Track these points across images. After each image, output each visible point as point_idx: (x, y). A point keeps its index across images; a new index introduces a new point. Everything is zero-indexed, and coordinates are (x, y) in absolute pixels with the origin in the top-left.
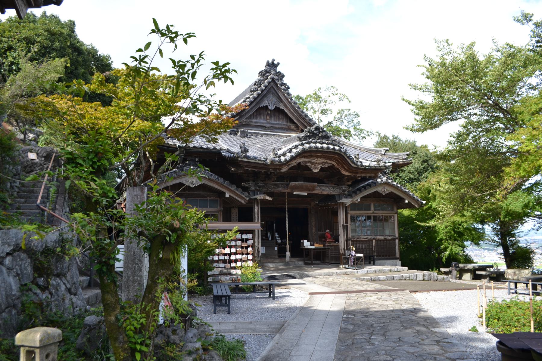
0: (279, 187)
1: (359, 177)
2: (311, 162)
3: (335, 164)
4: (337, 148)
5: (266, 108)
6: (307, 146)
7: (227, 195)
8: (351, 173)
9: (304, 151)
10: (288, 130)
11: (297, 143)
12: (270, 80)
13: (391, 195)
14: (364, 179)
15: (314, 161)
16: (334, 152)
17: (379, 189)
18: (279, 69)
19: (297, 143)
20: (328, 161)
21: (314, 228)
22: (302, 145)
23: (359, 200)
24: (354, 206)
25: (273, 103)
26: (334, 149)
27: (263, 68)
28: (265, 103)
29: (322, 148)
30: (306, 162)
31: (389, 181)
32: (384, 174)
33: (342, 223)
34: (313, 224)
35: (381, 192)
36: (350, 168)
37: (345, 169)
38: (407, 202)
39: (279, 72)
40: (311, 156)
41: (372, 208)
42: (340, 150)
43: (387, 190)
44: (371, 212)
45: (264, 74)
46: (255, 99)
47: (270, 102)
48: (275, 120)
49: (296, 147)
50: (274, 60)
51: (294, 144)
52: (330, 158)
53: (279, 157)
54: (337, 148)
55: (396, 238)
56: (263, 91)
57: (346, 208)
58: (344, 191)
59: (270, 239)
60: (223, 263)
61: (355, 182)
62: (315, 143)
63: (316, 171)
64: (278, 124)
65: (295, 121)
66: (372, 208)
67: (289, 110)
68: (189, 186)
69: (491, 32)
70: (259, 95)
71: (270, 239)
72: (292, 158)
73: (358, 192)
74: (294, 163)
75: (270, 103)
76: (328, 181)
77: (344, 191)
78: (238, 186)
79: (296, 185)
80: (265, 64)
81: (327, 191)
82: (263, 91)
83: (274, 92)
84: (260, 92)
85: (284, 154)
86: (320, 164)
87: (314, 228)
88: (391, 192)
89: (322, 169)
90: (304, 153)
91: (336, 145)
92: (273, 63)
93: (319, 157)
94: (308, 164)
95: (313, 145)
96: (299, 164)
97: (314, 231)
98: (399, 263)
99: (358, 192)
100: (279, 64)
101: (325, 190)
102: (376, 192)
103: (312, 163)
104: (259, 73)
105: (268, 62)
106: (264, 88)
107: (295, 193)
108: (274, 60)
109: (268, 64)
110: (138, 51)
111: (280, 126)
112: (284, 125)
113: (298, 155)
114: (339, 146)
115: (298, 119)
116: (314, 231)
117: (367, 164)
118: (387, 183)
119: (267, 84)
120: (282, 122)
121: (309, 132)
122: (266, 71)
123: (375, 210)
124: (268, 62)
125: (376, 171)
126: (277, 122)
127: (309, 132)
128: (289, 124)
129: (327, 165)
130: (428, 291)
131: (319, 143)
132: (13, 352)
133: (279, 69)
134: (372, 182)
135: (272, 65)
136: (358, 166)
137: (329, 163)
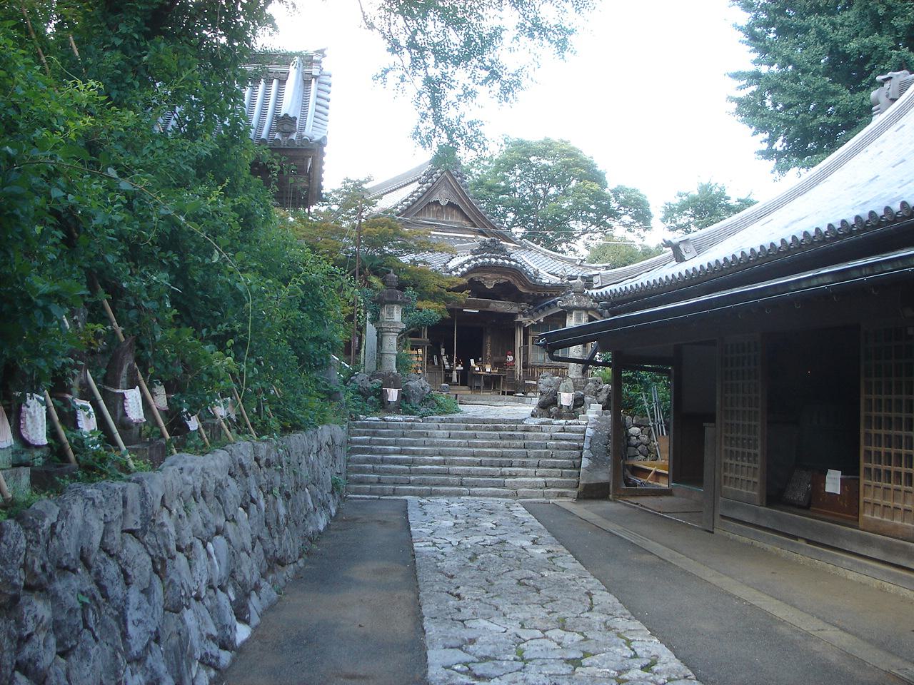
3: (510, 279)
4: (513, 263)
5: (437, 203)
6: (481, 261)
9: (476, 267)
11: (470, 257)
16: (510, 267)
19: (470, 257)
22: (475, 259)
24: (536, 327)
26: (510, 264)
28: (436, 198)
30: (479, 278)
36: (527, 285)
46: (424, 193)
48: (447, 218)
49: (469, 262)
51: (466, 258)
52: (506, 274)
53: (450, 272)
54: (513, 263)
59: (436, 364)
64: (451, 223)
70: (428, 188)
71: (436, 364)
72: (464, 274)
75: (442, 197)
84: (430, 184)
85: (456, 269)
89: (496, 285)
90: (476, 269)
91: (513, 260)
94: (482, 280)
95: (487, 260)
97: (488, 354)
99: (540, 311)
103: (486, 279)
106: (435, 180)
110: (293, 4)
113: (470, 271)
114: (516, 261)
116: (488, 354)
119: (439, 175)
120: (456, 220)
125: (558, 289)
128: (464, 222)
129: (502, 281)
131: (494, 257)
132: (0, 146)
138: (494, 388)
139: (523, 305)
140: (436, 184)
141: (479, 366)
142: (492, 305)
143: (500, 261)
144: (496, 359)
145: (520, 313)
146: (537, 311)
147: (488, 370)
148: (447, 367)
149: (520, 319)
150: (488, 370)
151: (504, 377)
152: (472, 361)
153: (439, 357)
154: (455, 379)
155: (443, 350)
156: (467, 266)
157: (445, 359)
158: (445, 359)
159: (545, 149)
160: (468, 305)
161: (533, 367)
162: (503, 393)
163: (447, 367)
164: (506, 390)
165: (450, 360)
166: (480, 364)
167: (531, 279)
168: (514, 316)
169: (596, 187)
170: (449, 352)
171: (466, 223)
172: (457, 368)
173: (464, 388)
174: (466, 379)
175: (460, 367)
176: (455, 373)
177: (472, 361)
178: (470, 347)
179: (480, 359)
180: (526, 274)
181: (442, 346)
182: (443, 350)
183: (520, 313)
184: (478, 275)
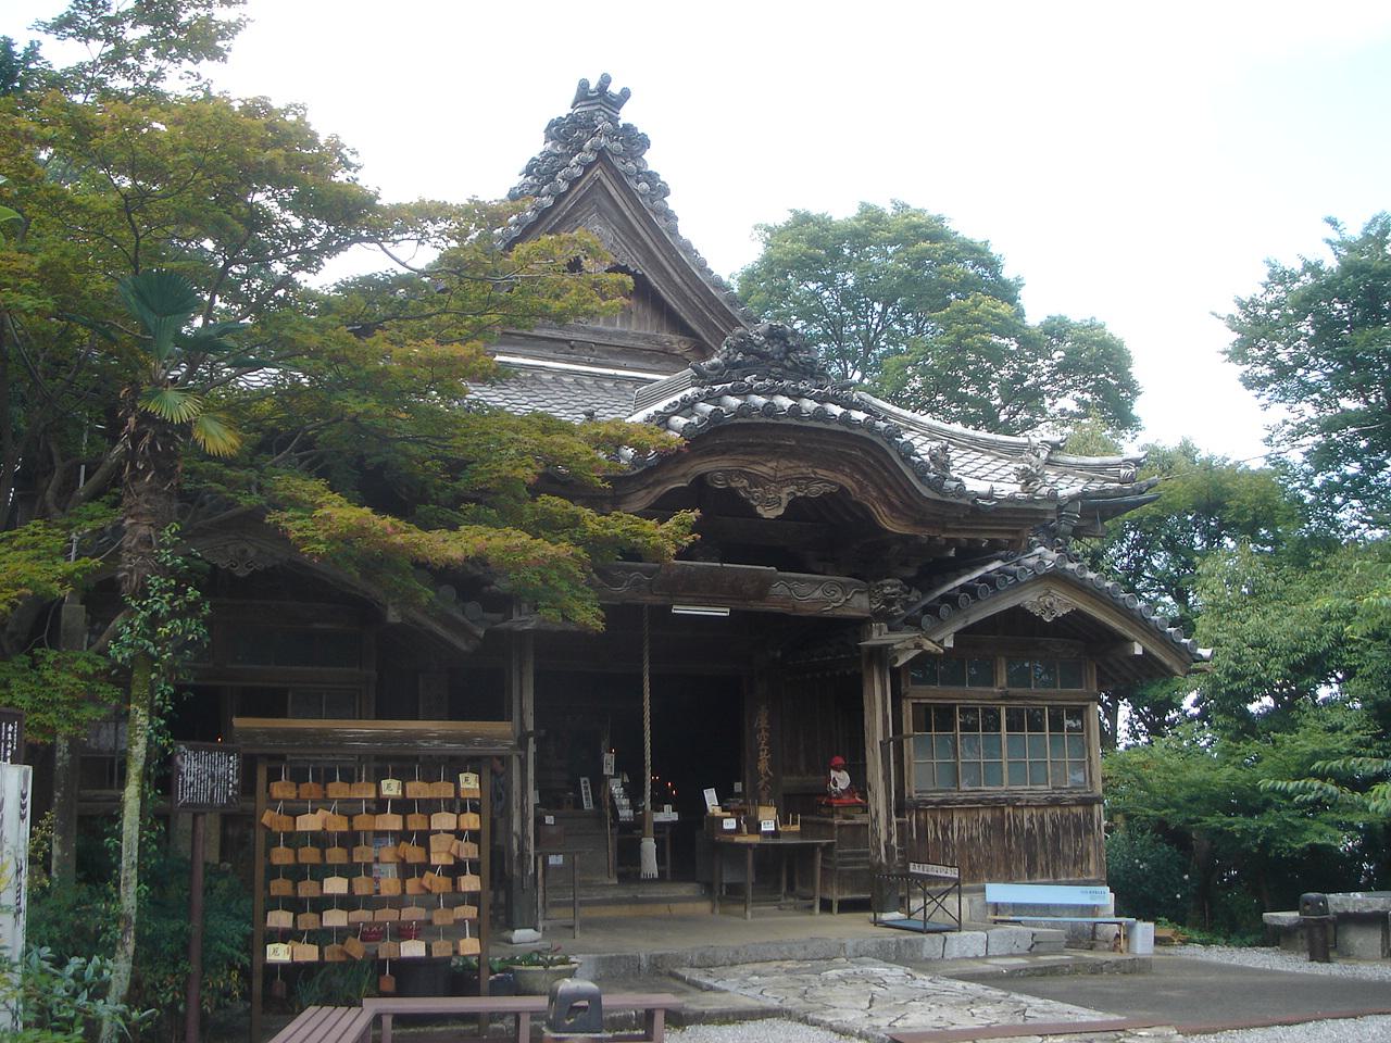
1: (950, 543)
2: (748, 475)
3: (849, 483)
4: (859, 416)
8: (917, 523)
10: (662, 357)
12: (591, 157)
13: (1075, 628)
14: (972, 556)
15: (764, 469)
17: (1030, 599)
18: (626, 115)
20: (821, 472)
21: (763, 756)
23: (949, 644)
27: (563, 108)
29: (795, 411)
30: (728, 473)
31: (1069, 566)
32: (1052, 537)
33: (879, 737)
35: (1037, 612)
36: (909, 504)
37: (891, 506)
38: (1138, 650)
39: (628, 128)
41: (1002, 679)
42: (871, 427)
43: (1061, 603)
45: (560, 131)
49: (686, 407)
50: (606, 80)
56: (559, 198)
57: (896, 674)
58: (889, 603)
59: (588, 805)
60: (341, 908)
61: (934, 568)
62: (769, 392)
63: (769, 513)
64: (623, 335)
65: (695, 326)
66: (1002, 679)
67: (669, 279)
69: (1303, 230)
71: (588, 805)
73: (944, 609)
77: (889, 603)
80: (572, 94)
82: (559, 198)
83: (606, 204)
84: (548, 201)
87: (763, 756)
88: (1077, 613)
89: (794, 504)
90: (713, 437)
91: (857, 407)
94: (740, 483)
97: (763, 766)
98: (1307, 955)
99: (944, 609)
101: (814, 593)
102: (1019, 611)
103: (755, 480)
104: (551, 125)
105: (584, 85)
106: (564, 187)
107: (678, 610)
108: (606, 80)
109: (583, 94)
111: (629, 343)
112: (646, 337)
115: (701, 318)
116: (763, 766)
117: (981, 487)
118: (1057, 577)
119: (578, 172)
121: (740, 347)
122: (573, 118)
123: (1010, 683)
124: (584, 85)
126: (618, 327)
127: (740, 347)
129: (816, 490)
130: (1248, 1027)
133: (626, 115)
134: (999, 570)
135: (599, 101)
136: (945, 494)
137: (823, 481)
138: (791, 887)
139: (890, 587)
140: (568, 203)
141: (736, 813)
142: (778, 589)
143: (809, 405)
144: (791, 781)
145: (878, 616)
146: (931, 610)
147: (768, 826)
148: (626, 814)
149: (878, 636)
150: (768, 826)
151: (828, 849)
152: (710, 796)
153: (599, 782)
154: (650, 866)
155: (609, 759)
156: (679, 421)
157: (616, 788)
158: (616, 788)
159: (868, 229)
160: (692, 588)
161: (918, 807)
162: (826, 906)
163: (626, 814)
164: (836, 896)
165: (634, 792)
166: (736, 803)
167: (922, 478)
168: (858, 625)
169: (1004, 309)
170: (629, 766)
171: (675, 338)
172: (660, 817)
173: (684, 890)
174: (691, 852)
175: (668, 815)
176: (649, 846)
177: (710, 796)
178: (701, 752)
179: (738, 787)
180: (906, 459)
181: (605, 744)
182: (609, 759)
183: (878, 616)
184: (724, 463)
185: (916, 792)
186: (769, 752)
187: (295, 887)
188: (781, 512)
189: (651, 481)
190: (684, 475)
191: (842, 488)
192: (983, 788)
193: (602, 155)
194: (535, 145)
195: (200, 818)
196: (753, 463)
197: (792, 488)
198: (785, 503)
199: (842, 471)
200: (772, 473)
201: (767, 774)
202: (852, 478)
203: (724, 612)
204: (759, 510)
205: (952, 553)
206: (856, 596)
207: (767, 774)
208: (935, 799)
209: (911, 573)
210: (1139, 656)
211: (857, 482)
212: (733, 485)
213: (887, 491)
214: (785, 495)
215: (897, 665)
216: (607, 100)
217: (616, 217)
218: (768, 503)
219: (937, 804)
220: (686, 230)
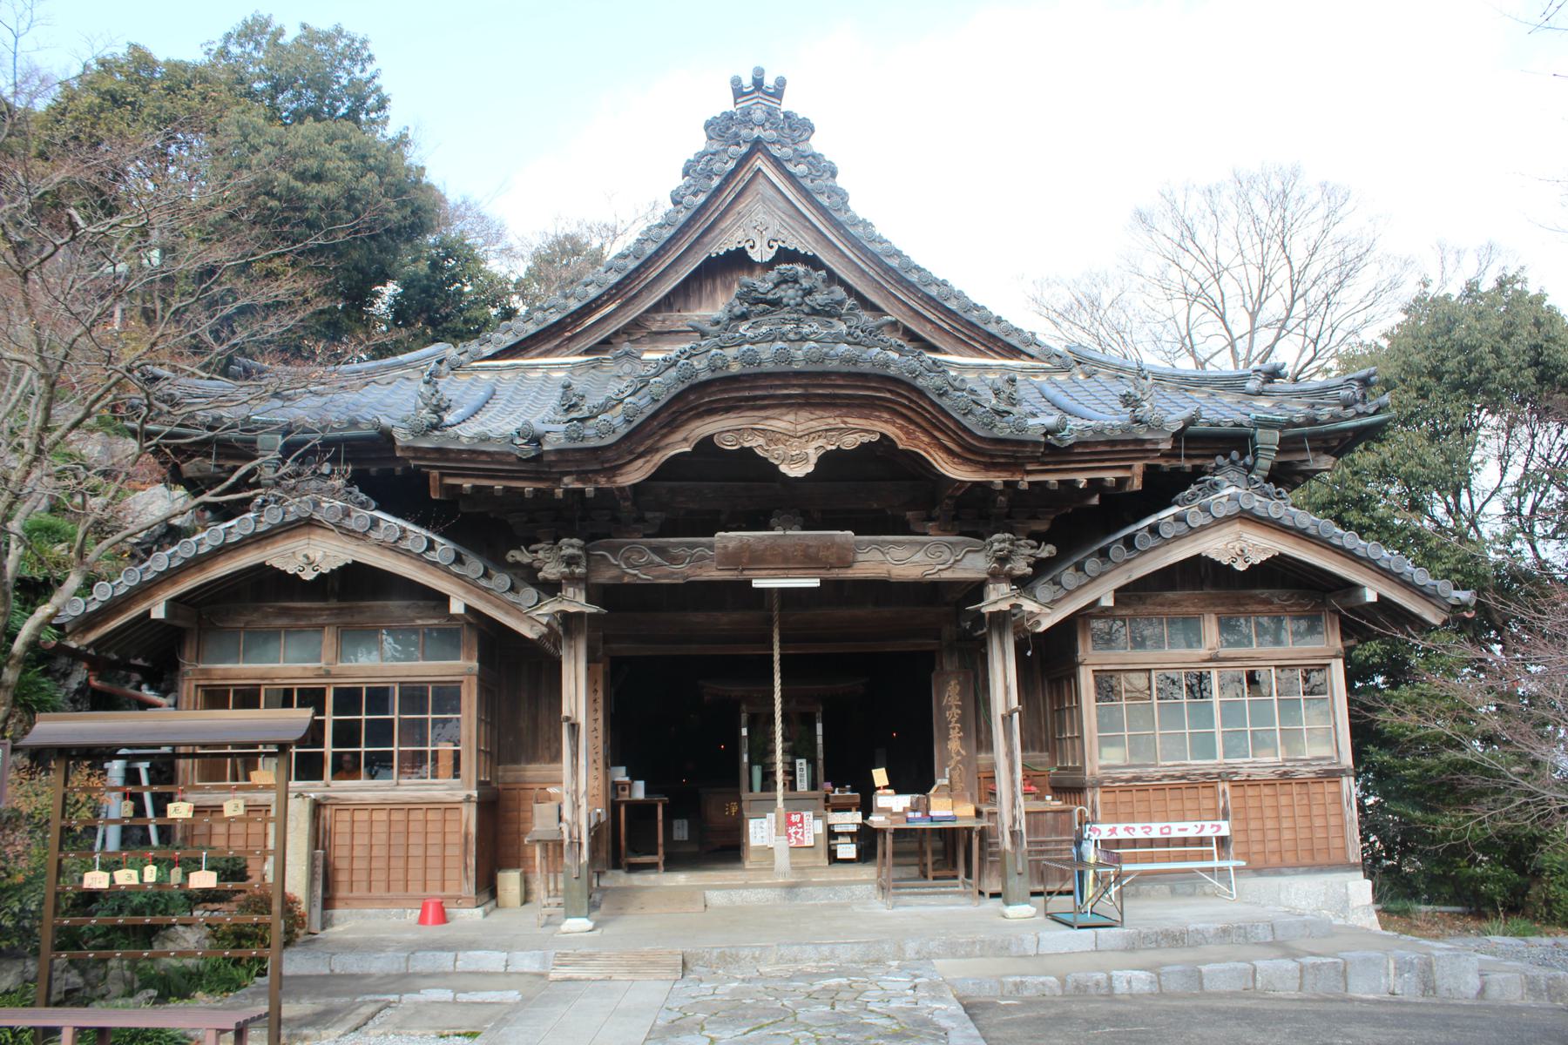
0: (674, 560)
3: (891, 431)
5: (738, 260)
7: (456, 607)
8: (989, 467)
20: (853, 422)
23: (1108, 601)
25: (768, 235)
34: (953, 714)
36: (972, 449)
39: (787, 116)
40: (752, 404)
44: (1204, 652)
45: (719, 128)
47: (753, 235)
52: (867, 406)
55: (1343, 771)
68: (296, 575)
74: (680, 444)
76: (930, 519)
78: (495, 559)
79: (744, 548)
81: (917, 564)
83: (770, 192)
86: (810, 435)
88: (1281, 554)
92: (758, 84)
93: (801, 406)
94: (755, 442)
96: (707, 442)
99: (1092, 565)
100: (781, 83)
102: (1198, 560)
103: (772, 437)
107: (757, 584)
129: (850, 442)
135: (759, 90)
149: (998, 598)
168: (976, 590)
185: (435, 753)
186: (961, 730)
187: (112, 881)
188: (810, 469)
189: (642, 449)
190: (685, 440)
191: (882, 435)
192: (1189, 761)
193: (757, 146)
194: (698, 142)
195: (837, 829)
196: (767, 418)
197: (821, 442)
198: (813, 460)
199: (879, 418)
200: (791, 427)
201: (958, 753)
202: (894, 424)
203: (814, 583)
204: (783, 469)
205: (1095, 501)
206: (970, 556)
207: (958, 753)
208: (1125, 776)
209: (1042, 526)
210: (1372, 604)
211: (901, 428)
212: (747, 445)
213: (937, 434)
214: (813, 452)
215: (1041, 629)
216: (765, 93)
217: (782, 204)
218: (793, 460)
219: (1127, 781)
220: (861, 205)
